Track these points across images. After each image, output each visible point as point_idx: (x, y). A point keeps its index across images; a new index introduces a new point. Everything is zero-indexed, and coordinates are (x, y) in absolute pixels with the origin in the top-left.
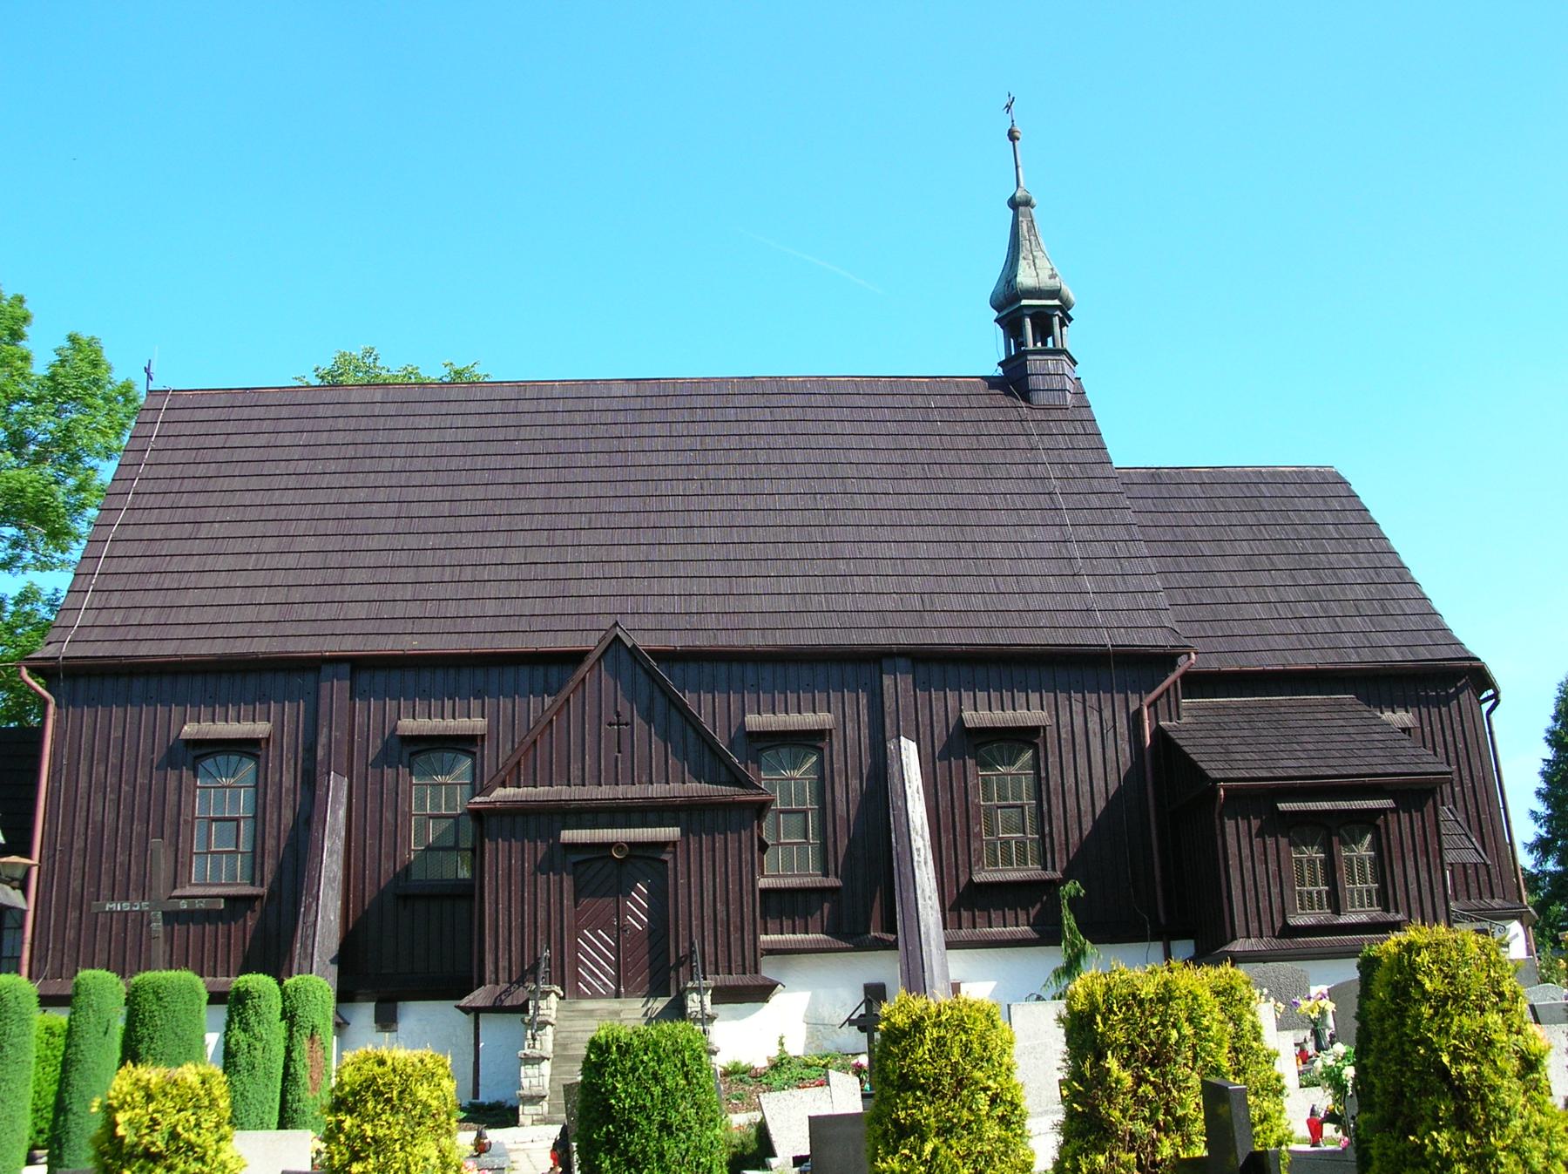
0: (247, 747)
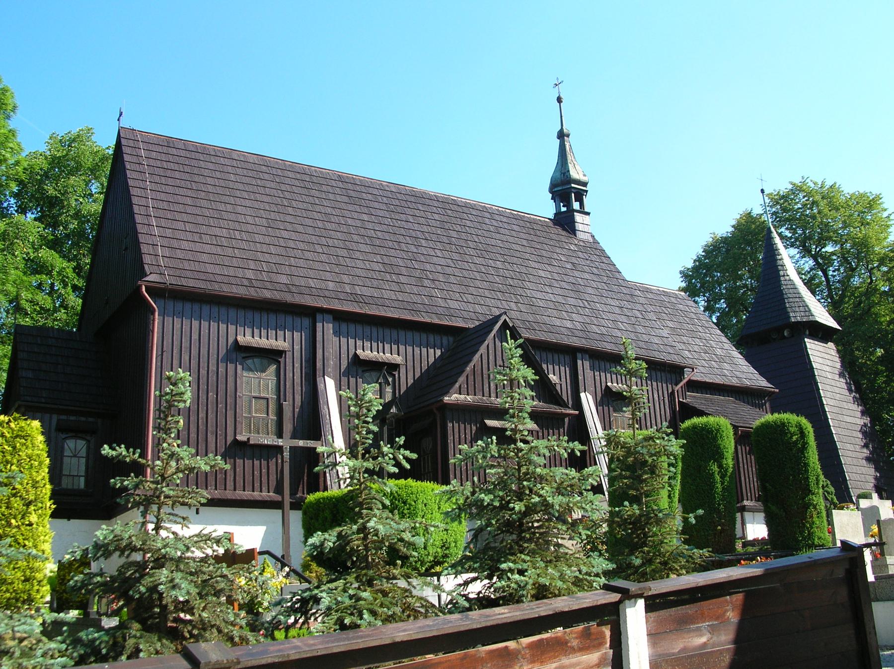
0: (273, 356)
